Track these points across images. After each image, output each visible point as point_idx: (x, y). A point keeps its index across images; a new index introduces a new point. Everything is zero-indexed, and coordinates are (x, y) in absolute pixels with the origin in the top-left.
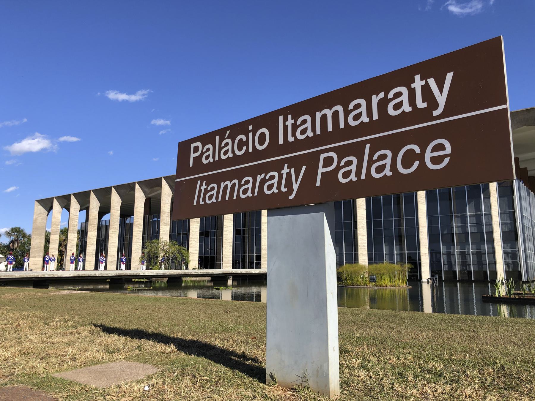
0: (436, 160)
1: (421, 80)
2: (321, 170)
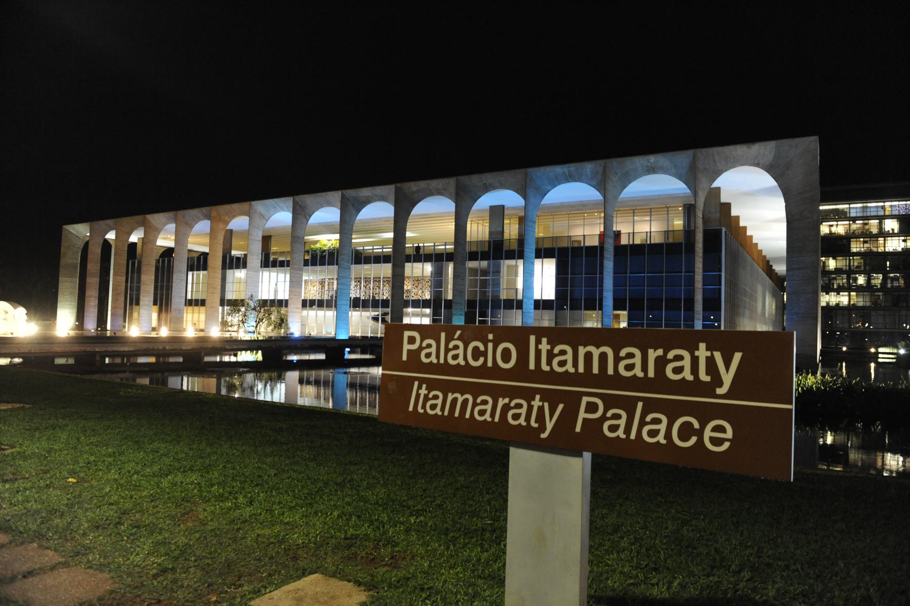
0: (714, 441)
1: (707, 350)
2: (582, 415)
